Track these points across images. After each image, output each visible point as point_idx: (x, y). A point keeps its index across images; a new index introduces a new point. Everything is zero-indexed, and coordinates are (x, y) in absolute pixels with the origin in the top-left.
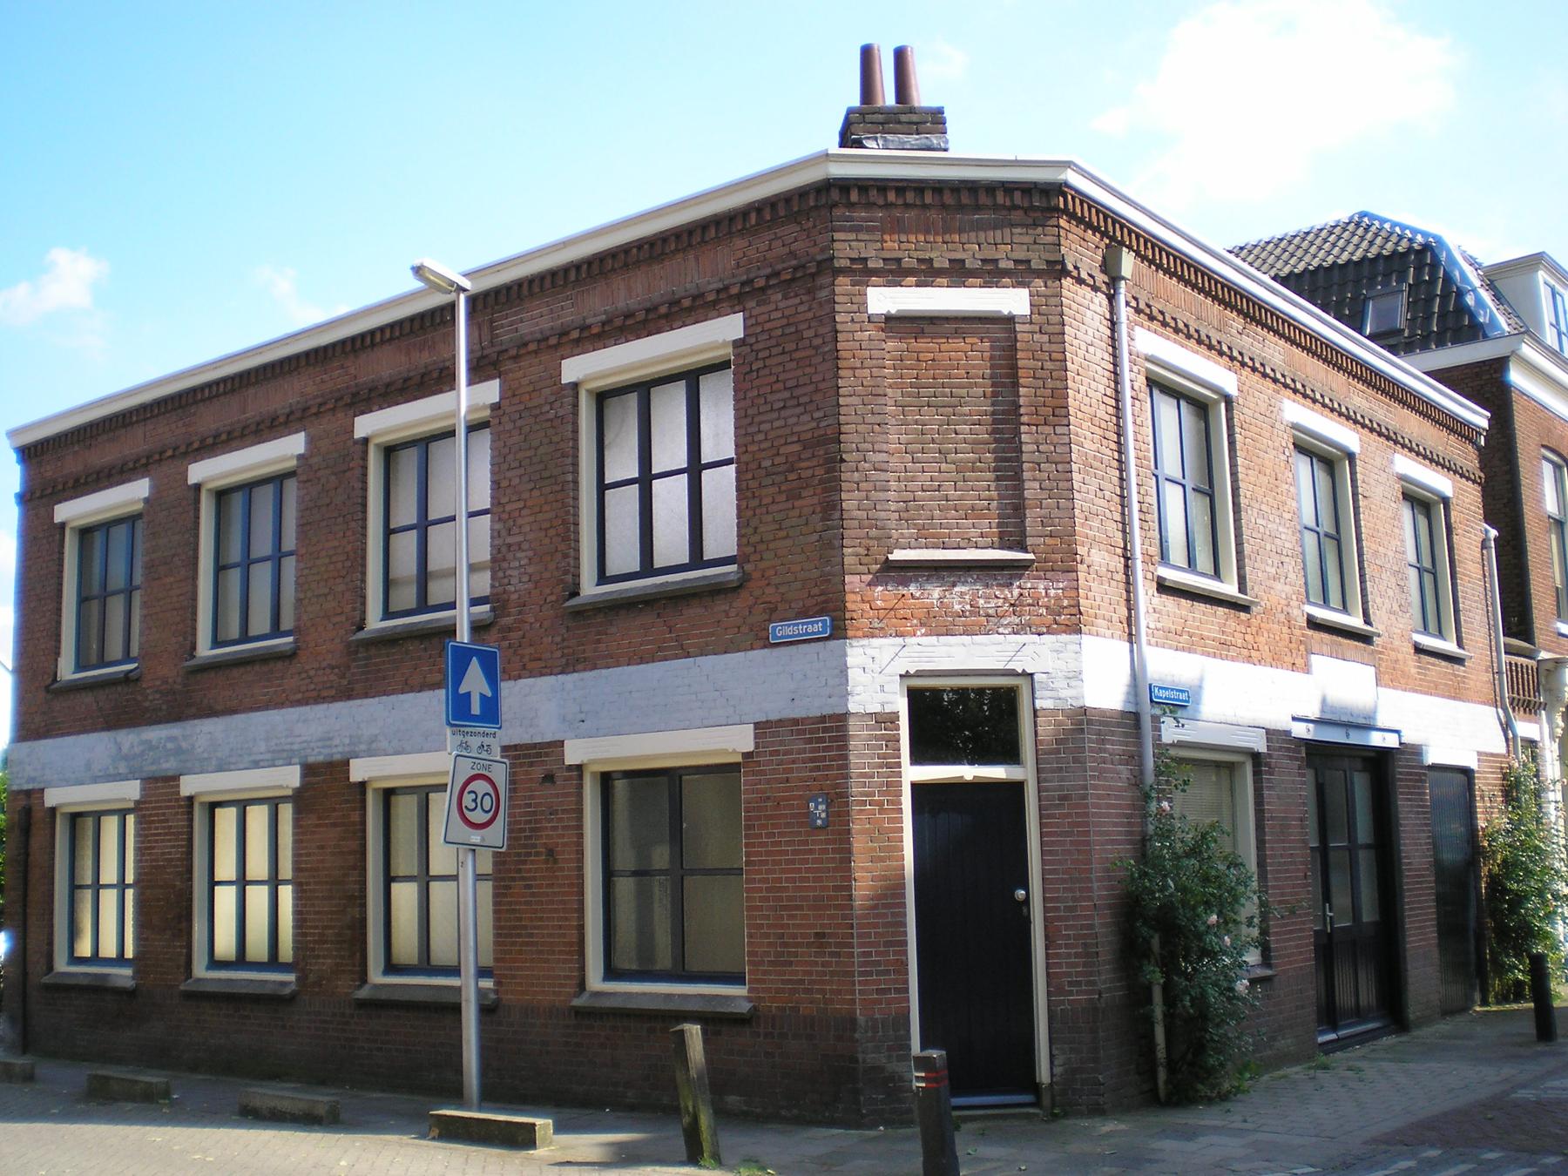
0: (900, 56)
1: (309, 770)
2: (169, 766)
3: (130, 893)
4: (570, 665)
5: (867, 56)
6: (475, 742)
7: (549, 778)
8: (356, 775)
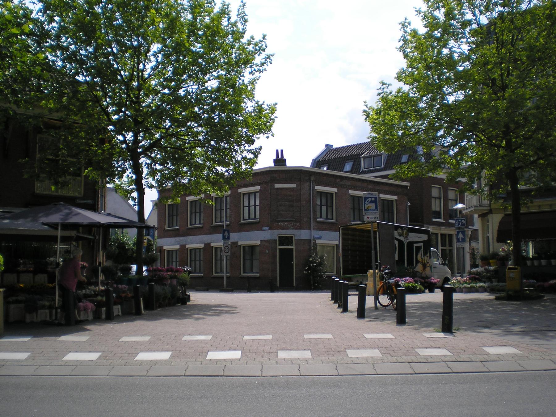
0: (282, 151)
1: (205, 244)
2: (184, 243)
3: (178, 263)
4: (240, 231)
5: (277, 151)
6: (226, 242)
7: (236, 247)
8: (211, 245)
